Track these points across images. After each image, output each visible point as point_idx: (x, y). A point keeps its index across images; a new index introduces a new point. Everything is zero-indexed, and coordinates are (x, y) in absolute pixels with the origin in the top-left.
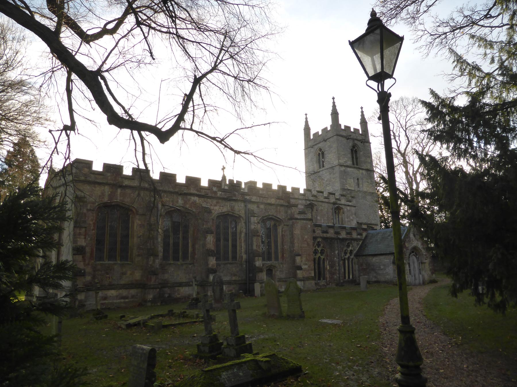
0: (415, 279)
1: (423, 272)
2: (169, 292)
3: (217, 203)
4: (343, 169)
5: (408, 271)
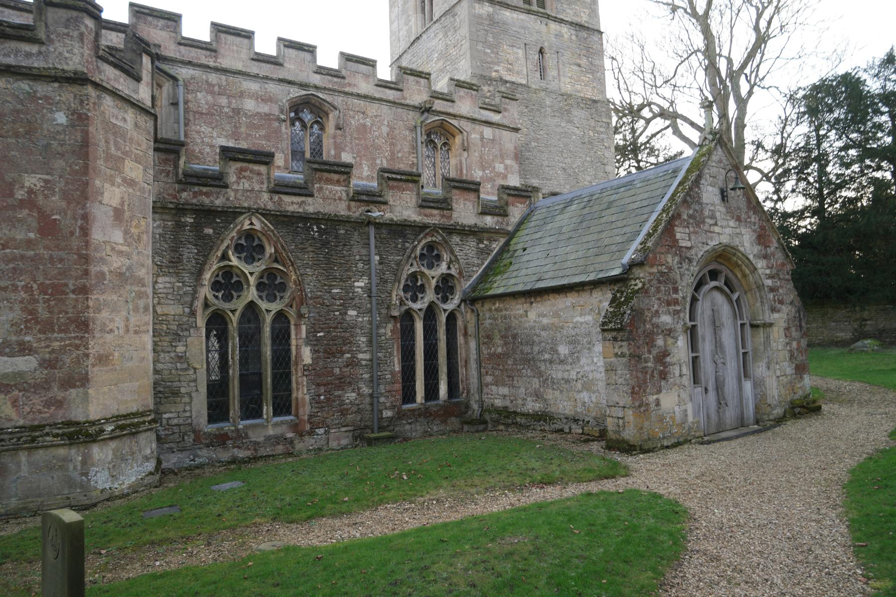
0: (721, 401)
1: (760, 369)
5: (686, 370)
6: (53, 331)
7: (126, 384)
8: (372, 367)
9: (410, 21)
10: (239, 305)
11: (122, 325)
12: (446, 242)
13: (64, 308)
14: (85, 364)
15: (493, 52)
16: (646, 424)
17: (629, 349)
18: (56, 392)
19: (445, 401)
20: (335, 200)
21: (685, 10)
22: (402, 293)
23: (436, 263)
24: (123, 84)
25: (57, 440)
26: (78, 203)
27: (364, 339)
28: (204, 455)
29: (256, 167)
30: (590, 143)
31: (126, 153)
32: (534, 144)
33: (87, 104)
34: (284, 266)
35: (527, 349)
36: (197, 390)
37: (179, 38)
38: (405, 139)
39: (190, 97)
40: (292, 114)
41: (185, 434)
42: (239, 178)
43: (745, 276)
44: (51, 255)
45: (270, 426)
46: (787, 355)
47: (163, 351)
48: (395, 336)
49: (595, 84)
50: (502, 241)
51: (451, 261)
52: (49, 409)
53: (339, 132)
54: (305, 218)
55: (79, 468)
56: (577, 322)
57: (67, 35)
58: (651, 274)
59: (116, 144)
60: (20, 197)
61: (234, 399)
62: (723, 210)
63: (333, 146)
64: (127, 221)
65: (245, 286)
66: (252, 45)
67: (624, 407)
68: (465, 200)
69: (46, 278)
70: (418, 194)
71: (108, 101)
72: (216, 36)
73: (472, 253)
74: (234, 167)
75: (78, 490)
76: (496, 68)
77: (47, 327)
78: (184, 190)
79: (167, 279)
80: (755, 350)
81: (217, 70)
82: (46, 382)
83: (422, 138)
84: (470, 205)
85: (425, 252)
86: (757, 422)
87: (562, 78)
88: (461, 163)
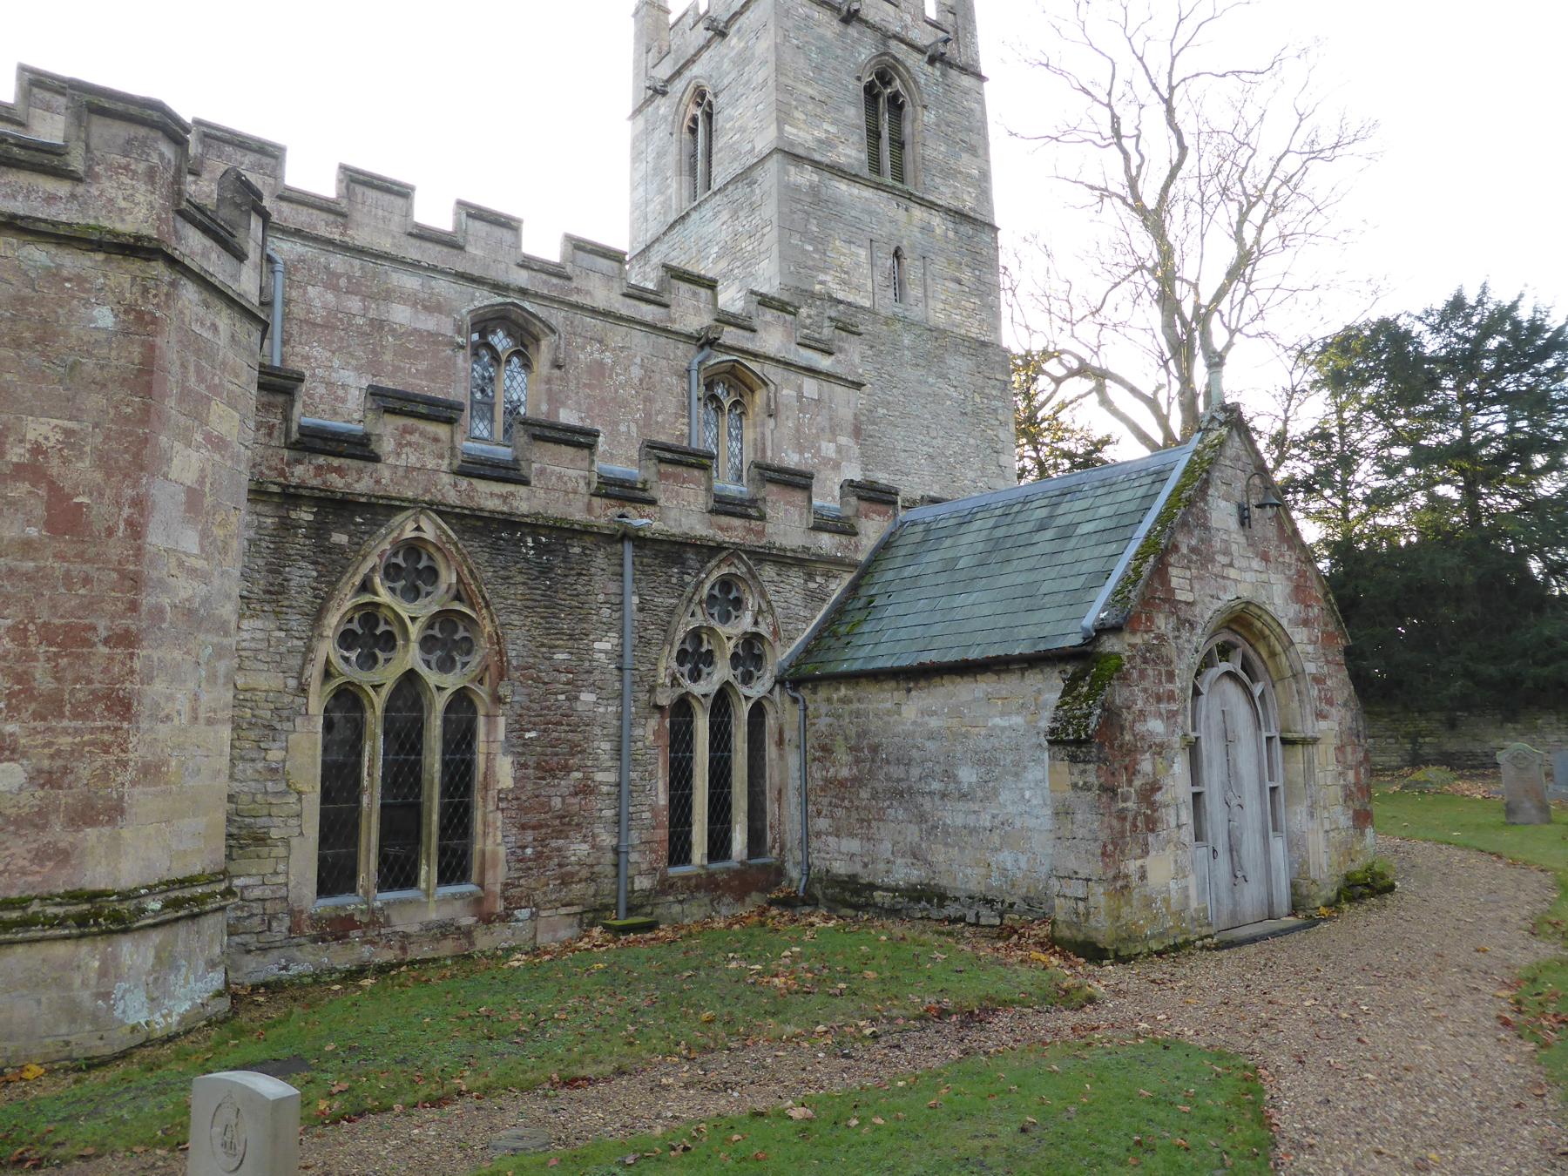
0: (1237, 875)
1: (1297, 818)
4: (805, 177)
5: (1186, 816)
6: (62, 715)
7: (187, 821)
8: (619, 797)
9: (669, 186)
10: (388, 673)
12: (754, 577)
13: (84, 671)
14: (119, 780)
15: (816, 250)
16: (1125, 910)
17: (1098, 777)
18: (58, 832)
19: (742, 863)
20: (566, 493)
21: (1124, 200)
22: (674, 665)
23: (734, 613)
24: (215, 264)
26: (126, 476)
27: (606, 746)
30: (975, 414)
32: (881, 411)
33: (155, 296)
35: (897, 772)
36: (301, 834)
38: (670, 391)
40: (475, 337)
41: (274, 916)
42: (400, 445)
43: (1273, 654)
44: (68, 570)
45: (430, 903)
46: (1340, 793)
48: (660, 743)
49: (984, 315)
50: (847, 578)
51: (760, 611)
52: (42, 866)
53: (556, 372)
54: (509, 523)
55: (93, 982)
56: (995, 726)
57: (126, 168)
58: (1132, 646)
59: (199, 370)
60: (15, 459)
61: (369, 851)
62: (1243, 540)
63: (544, 397)
64: (208, 513)
65: (400, 642)
67: (1088, 880)
68: (788, 503)
69: (55, 615)
70: (709, 489)
71: (190, 293)
72: (348, 188)
73: (796, 598)
75: (88, 1027)
76: (822, 277)
77: (53, 706)
78: (299, 462)
79: (259, 623)
80: (1289, 783)
81: (345, 248)
82: (40, 813)
83: (699, 391)
84: (795, 514)
85: (716, 592)
86: (1295, 909)
87: (930, 302)
88: (763, 438)
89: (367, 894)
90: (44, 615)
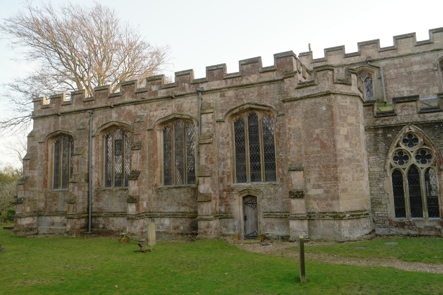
2: (103, 223)
3: (158, 106)
6: (327, 181)
11: (351, 178)
18: (329, 201)
25: (330, 218)
28: (394, 230)
29: (410, 104)
31: (348, 114)
34: (429, 147)
36: (389, 203)
37: (379, 49)
39: (386, 73)
41: (385, 220)
47: (374, 186)
59: (343, 112)
65: (409, 158)
66: (415, 39)
71: (339, 97)
72: (396, 42)
74: (399, 106)
78: (377, 120)
79: (373, 157)
89: (409, 218)
90: (322, 163)
